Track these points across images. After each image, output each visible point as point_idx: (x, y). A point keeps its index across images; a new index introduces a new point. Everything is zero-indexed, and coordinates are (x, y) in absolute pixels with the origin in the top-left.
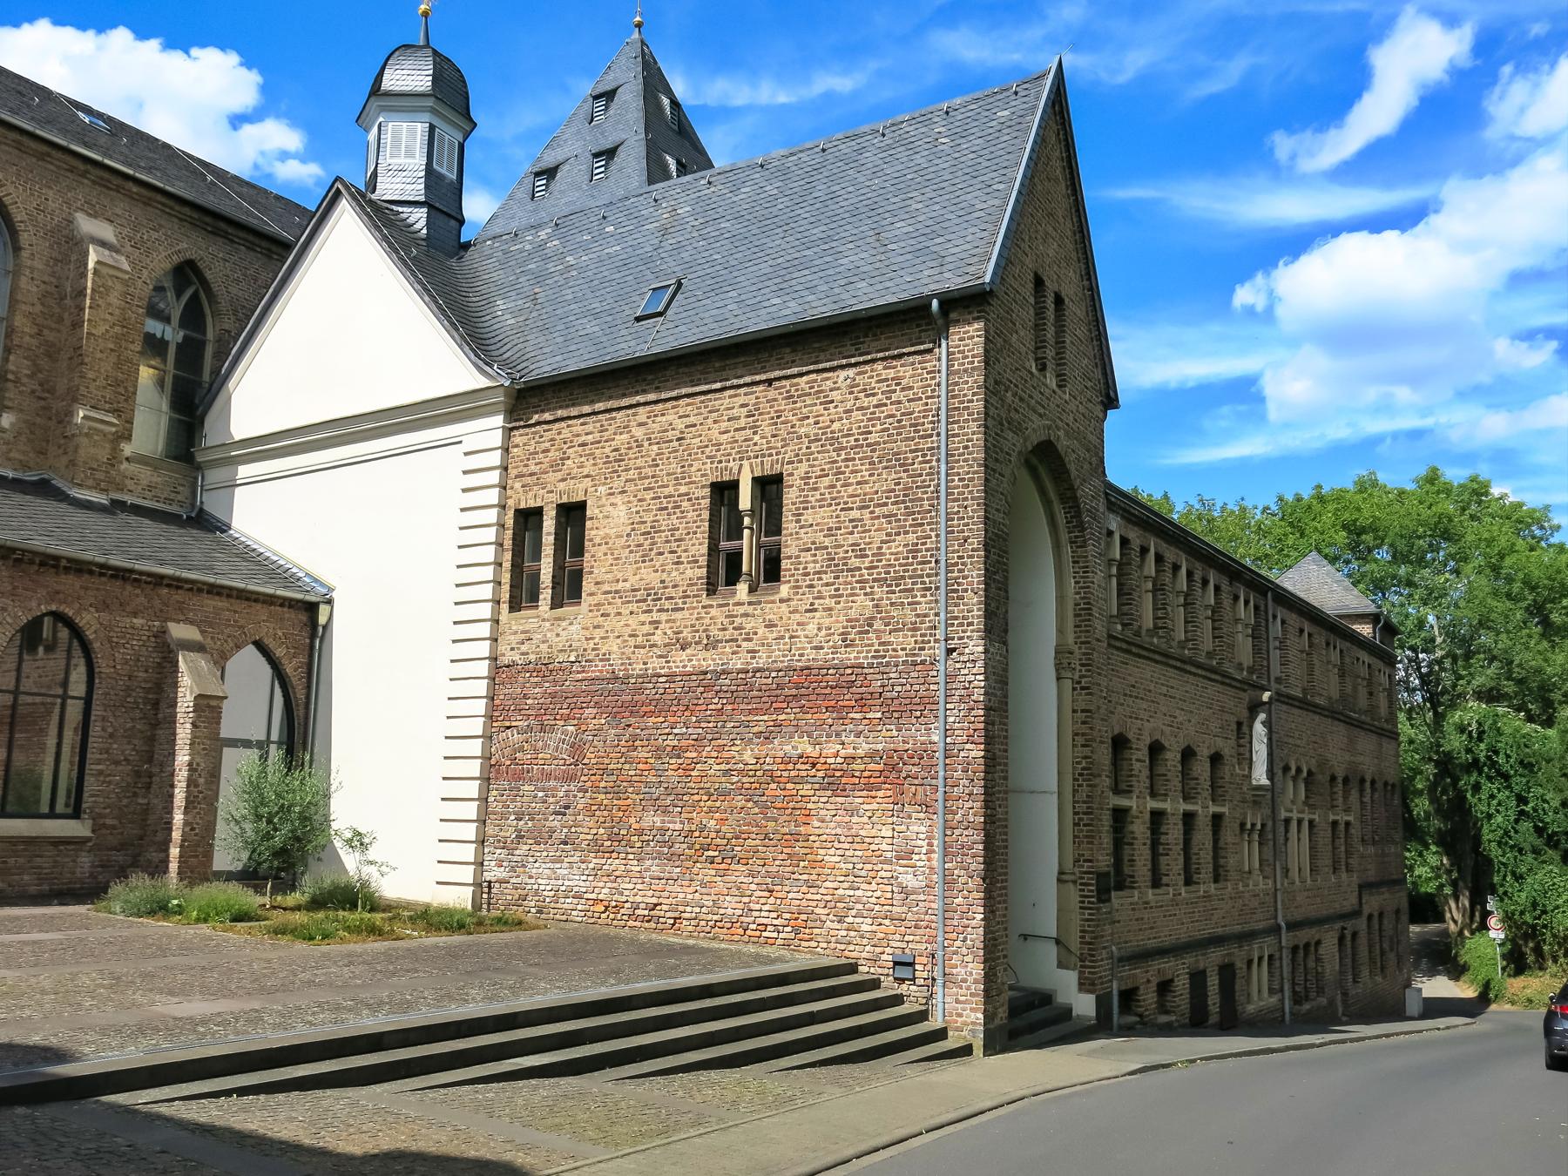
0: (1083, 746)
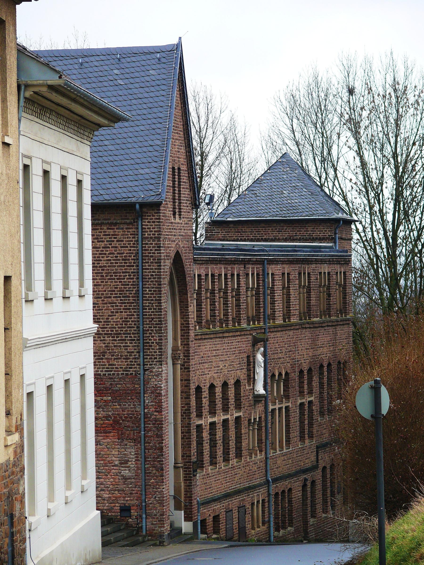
0: (185, 398)
